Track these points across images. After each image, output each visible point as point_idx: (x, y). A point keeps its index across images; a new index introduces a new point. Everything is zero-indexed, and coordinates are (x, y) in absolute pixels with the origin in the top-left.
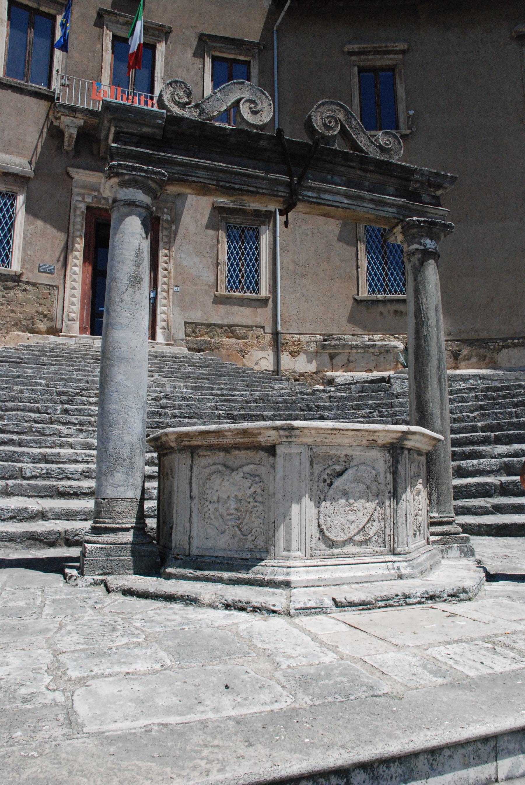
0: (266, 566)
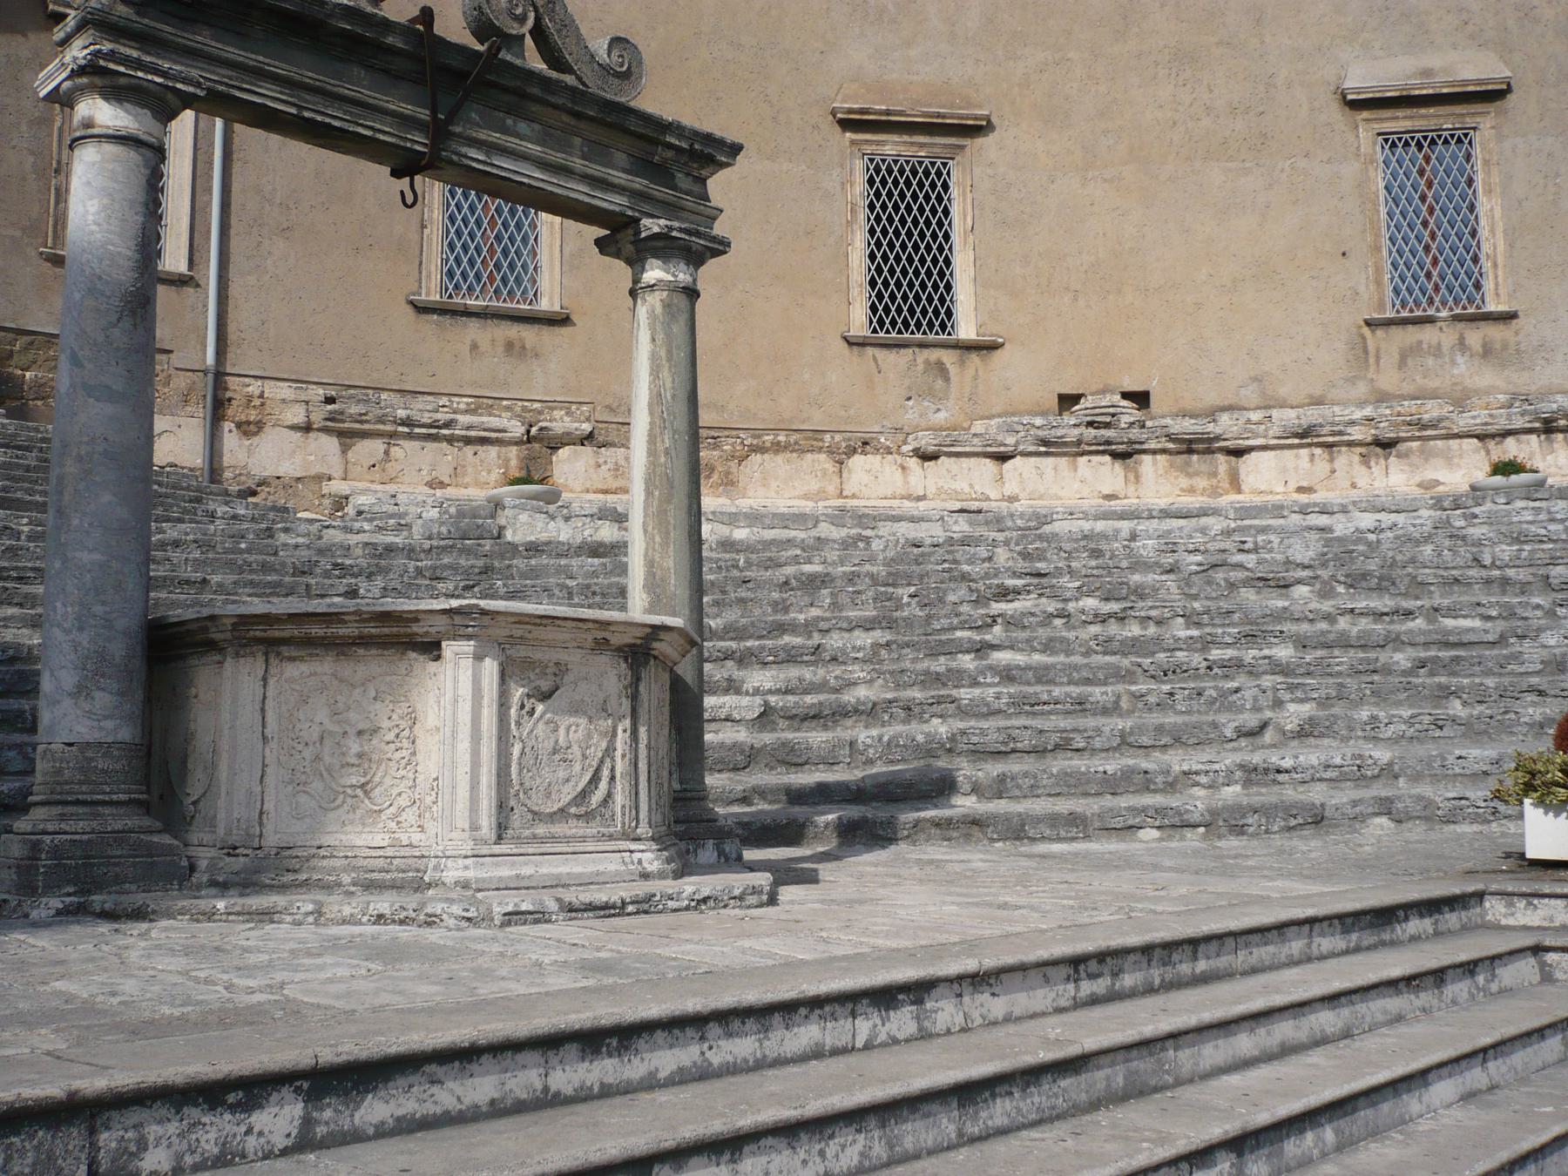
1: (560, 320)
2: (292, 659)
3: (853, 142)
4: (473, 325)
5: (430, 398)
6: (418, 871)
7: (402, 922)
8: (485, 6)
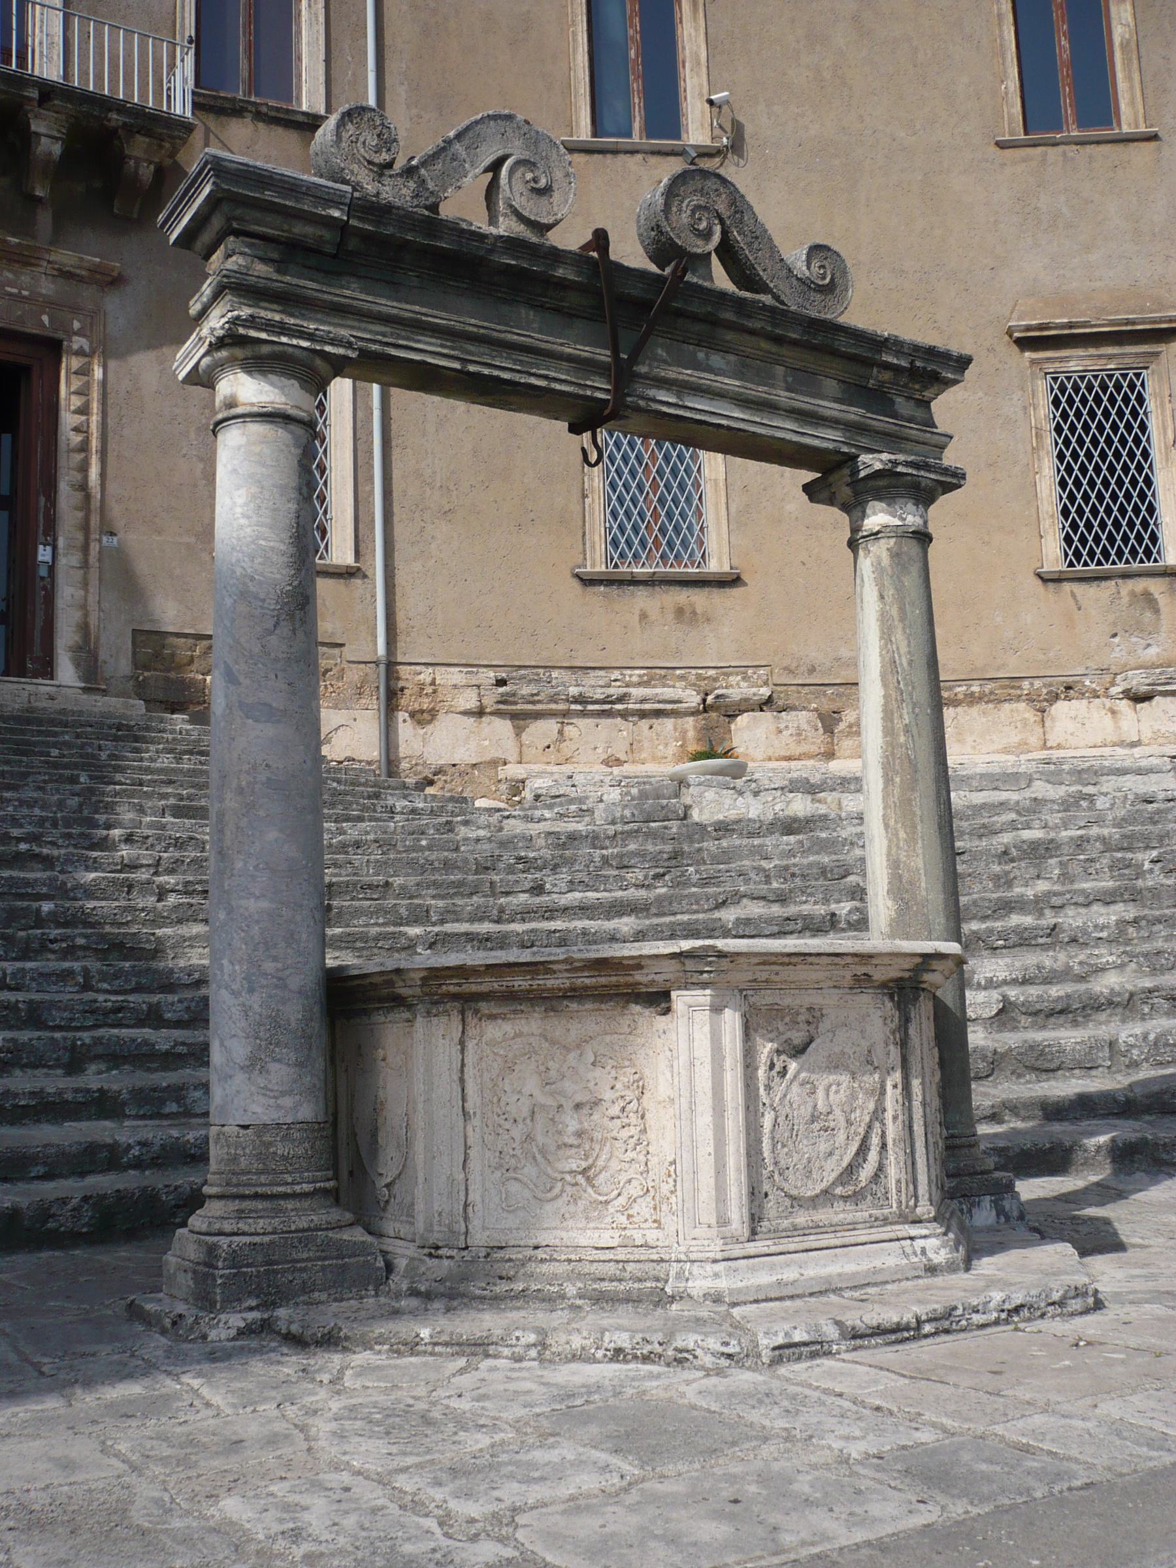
0: (662, 1260)
1: (731, 581)
2: (492, 1017)
3: (1033, 362)
4: (641, 593)
5: (602, 673)
6: (657, 1280)
7: (646, 1359)
8: (664, 223)
